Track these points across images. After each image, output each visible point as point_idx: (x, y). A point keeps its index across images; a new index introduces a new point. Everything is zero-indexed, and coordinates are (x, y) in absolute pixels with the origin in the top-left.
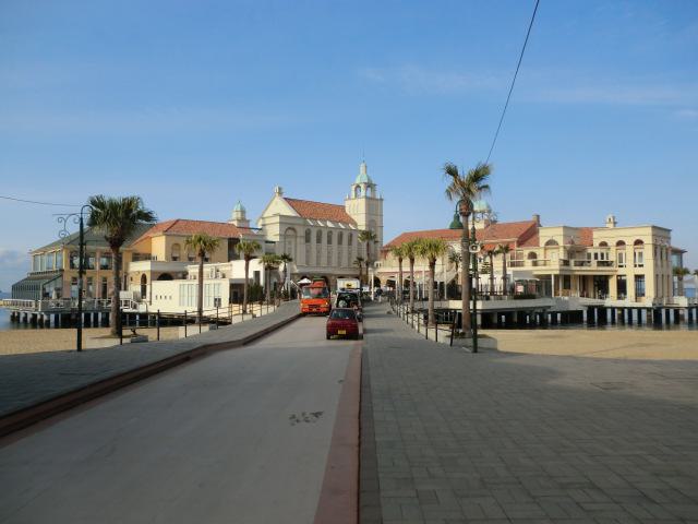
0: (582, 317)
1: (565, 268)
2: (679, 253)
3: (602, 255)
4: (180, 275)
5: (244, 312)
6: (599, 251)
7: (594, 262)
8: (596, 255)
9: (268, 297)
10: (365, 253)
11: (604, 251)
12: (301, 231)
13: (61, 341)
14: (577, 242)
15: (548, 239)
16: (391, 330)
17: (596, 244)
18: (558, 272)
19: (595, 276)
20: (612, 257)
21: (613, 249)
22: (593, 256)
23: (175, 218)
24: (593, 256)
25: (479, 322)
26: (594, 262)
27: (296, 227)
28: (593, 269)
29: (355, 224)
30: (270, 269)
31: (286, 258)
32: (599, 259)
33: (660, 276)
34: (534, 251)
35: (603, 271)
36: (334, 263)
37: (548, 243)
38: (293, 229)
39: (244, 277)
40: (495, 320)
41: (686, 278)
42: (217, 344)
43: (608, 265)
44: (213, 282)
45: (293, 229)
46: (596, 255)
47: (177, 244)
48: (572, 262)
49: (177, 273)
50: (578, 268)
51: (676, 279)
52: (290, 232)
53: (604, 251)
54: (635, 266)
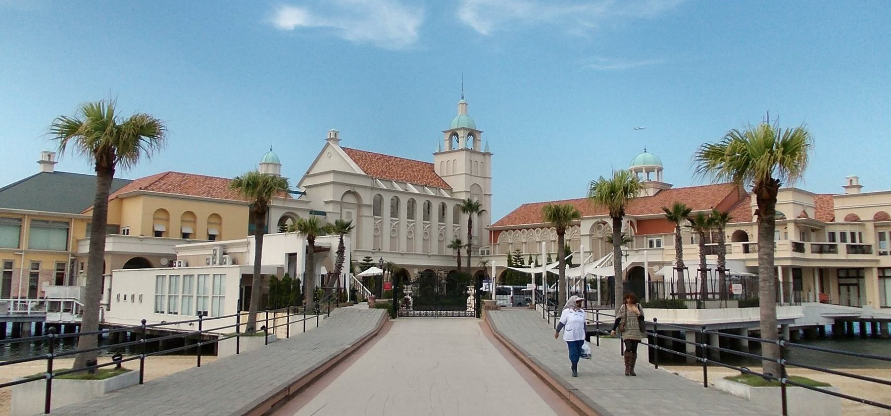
0: (441, 222)
1: (798, 255)
3: (853, 234)
4: (164, 261)
5: (251, 330)
6: (848, 230)
7: (842, 247)
8: (843, 235)
9: (308, 301)
10: (111, 198)
12: (367, 198)
14: (811, 214)
17: (840, 218)
18: (788, 263)
19: (839, 269)
20: (870, 239)
21: (870, 227)
23: (167, 171)
24: (838, 237)
26: (842, 247)
27: (358, 191)
28: (842, 257)
29: (449, 189)
30: (314, 253)
31: (343, 228)
32: (849, 242)
34: (743, 229)
35: (858, 260)
36: (403, 246)
38: (355, 194)
43: (863, 252)
45: (355, 194)
46: (843, 235)
47: (217, 216)
48: (807, 246)
49: (160, 256)
50: (817, 256)
52: (350, 199)
53: (856, 230)
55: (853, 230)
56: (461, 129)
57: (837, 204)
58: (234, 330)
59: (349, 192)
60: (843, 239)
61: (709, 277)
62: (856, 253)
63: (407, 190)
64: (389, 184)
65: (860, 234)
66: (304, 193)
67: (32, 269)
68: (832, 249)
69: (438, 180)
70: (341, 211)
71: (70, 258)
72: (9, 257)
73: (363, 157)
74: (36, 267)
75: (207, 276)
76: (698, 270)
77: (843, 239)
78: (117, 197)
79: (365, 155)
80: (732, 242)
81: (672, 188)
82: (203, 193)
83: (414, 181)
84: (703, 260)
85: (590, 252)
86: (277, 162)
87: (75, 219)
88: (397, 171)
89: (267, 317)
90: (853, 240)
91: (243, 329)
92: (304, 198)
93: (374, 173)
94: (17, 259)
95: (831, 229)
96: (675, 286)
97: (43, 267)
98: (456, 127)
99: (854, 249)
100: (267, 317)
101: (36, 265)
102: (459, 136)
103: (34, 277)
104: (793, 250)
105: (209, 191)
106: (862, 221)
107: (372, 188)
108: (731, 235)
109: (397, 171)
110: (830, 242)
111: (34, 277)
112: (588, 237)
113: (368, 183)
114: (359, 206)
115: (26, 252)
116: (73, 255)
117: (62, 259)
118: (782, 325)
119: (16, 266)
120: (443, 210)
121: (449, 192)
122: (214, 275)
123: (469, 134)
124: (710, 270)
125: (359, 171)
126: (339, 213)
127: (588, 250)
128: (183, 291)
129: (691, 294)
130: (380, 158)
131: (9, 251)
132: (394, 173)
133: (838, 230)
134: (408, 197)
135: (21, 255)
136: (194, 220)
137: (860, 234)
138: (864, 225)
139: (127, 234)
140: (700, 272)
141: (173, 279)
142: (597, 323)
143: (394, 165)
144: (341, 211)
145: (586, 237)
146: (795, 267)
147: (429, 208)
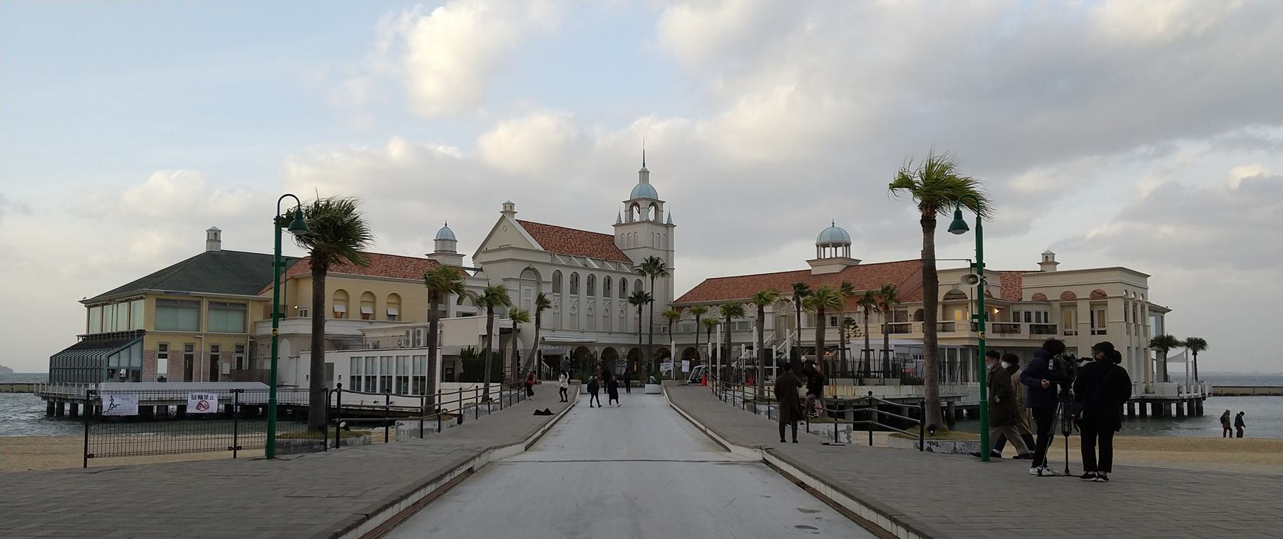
2: (1160, 311)
3: (1038, 314)
6: (1033, 310)
7: (1025, 327)
11: (1042, 309)
13: (437, 393)
15: (950, 288)
16: (816, 529)
17: (1027, 296)
18: (967, 343)
22: (1022, 317)
24: (1022, 317)
25: (998, 452)
26: (1025, 327)
33: (1133, 350)
37: (949, 296)
38: (534, 270)
39: (271, 251)
40: (450, 372)
41: (1172, 352)
42: (977, 225)
44: (411, 353)
50: (997, 336)
51: (1153, 354)
54: (1093, 333)
55: (1038, 310)
56: (642, 199)
57: (1026, 282)
58: (474, 400)
59: (528, 269)
60: (1028, 319)
61: (871, 357)
62: (1040, 333)
63: (586, 265)
64: (567, 259)
65: (1046, 314)
66: (481, 270)
67: (160, 350)
68: (1015, 329)
69: (618, 253)
70: (520, 288)
71: (249, 340)
72: (190, 341)
73: (540, 230)
74: (164, 349)
75: (406, 358)
76: (881, 350)
77: (1028, 319)
78: (292, 278)
79: (543, 229)
80: (914, 321)
81: (860, 264)
82: (381, 272)
83: (593, 256)
84: (886, 340)
85: (773, 330)
86: (452, 239)
87: (252, 300)
88: (575, 245)
89: (461, 398)
90: (1038, 319)
91: (480, 400)
92: (480, 274)
93: (552, 248)
94: (197, 341)
95: (1016, 308)
96: (863, 365)
97: (222, 349)
98: (636, 198)
99: (1037, 329)
100: (461, 398)
101: (215, 348)
102: (641, 207)
103: (214, 360)
104: (972, 330)
105: (386, 270)
106: (1049, 301)
107: (551, 264)
108: (913, 314)
109: (575, 245)
110: (1014, 321)
111: (214, 360)
112: (442, 422)
113: (548, 259)
114: (538, 283)
115: (206, 335)
116: (251, 337)
117: (241, 342)
118: (948, 403)
119: (196, 349)
120: (624, 285)
121: (630, 267)
122: (414, 356)
123: (652, 204)
124: (873, 350)
125: (539, 247)
126: (517, 291)
127: (771, 328)
128: (413, 371)
129: (875, 372)
130: (557, 231)
131: (188, 335)
132: (573, 247)
133: (1023, 310)
134: (588, 273)
135: (201, 338)
136: (373, 301)
137: (1046, 314)
138: (1050, 305)
139: (1240, 434)
140: (863, 353)
141: (370, 361)
142: (836, 420)
143: (573, 239)
144: (520, 288)
145: (441, 424)
146: (950, 347)
147: (609, 284)
